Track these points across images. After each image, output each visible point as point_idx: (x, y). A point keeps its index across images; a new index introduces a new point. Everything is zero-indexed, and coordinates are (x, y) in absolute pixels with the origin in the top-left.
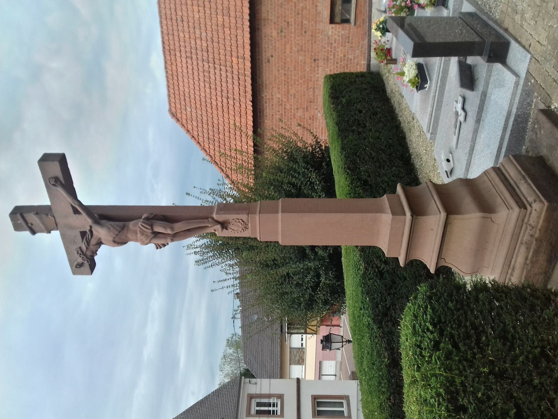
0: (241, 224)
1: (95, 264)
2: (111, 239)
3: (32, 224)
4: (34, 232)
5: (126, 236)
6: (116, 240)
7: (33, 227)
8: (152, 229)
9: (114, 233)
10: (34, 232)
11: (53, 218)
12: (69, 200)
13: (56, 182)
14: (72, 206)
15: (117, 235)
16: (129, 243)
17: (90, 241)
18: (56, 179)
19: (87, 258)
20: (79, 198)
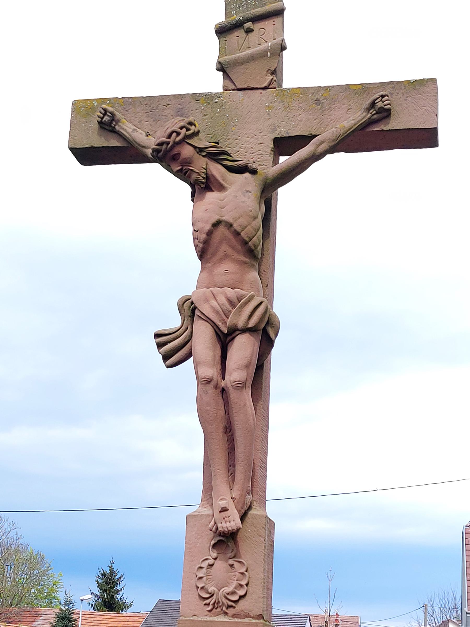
0: (233, 593)
1: (83, 165)
2: (227, 218)
3: (249, 31)
4: (222, 31)
5: (226, 256)
6: (222, 229)
7: (240, 33)
8: (245, 330)
9: (244, 228)
10: (222, 31)
11: (266, 84)
12: (328, 134)
13: (381, 110)
14: (315, 136)
15: (237, 234)
16: (199, 262)
17: (218, 161)
18: (386, 114)
19: (176, 144)
20: (328, 156)
